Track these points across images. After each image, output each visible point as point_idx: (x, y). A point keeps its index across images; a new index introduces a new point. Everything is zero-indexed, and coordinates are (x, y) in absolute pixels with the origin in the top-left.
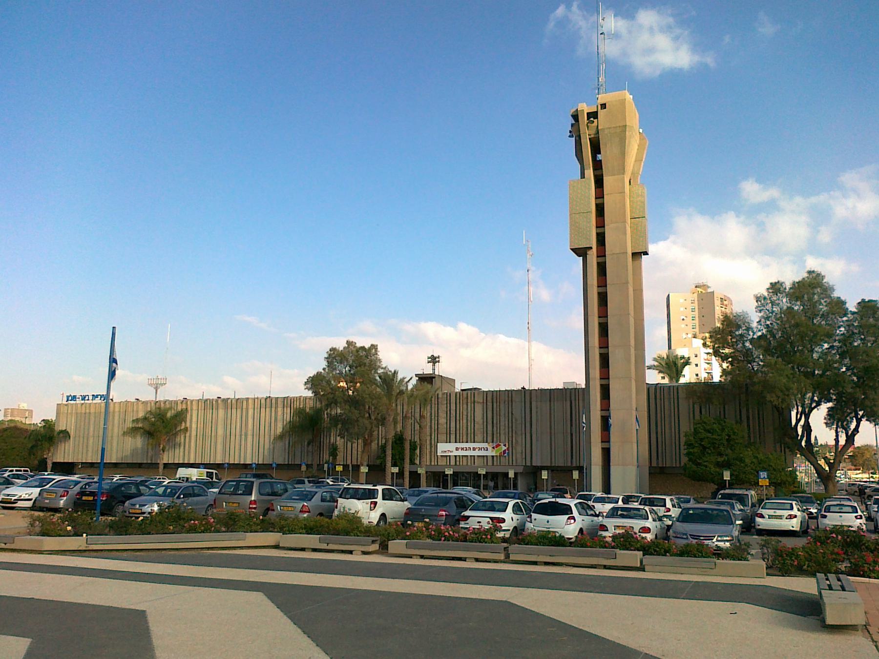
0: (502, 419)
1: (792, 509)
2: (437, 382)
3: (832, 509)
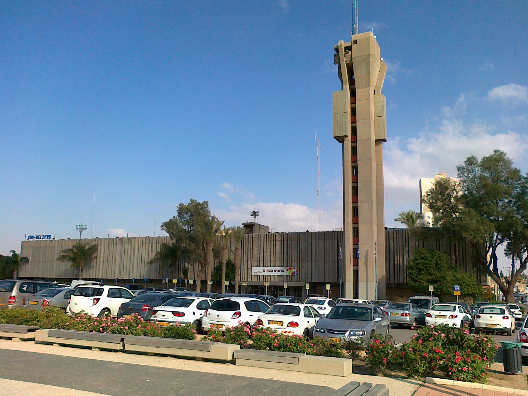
0: (293, 251)
1: (454, 310)
2: (255, 228)
3: (485, 311)
